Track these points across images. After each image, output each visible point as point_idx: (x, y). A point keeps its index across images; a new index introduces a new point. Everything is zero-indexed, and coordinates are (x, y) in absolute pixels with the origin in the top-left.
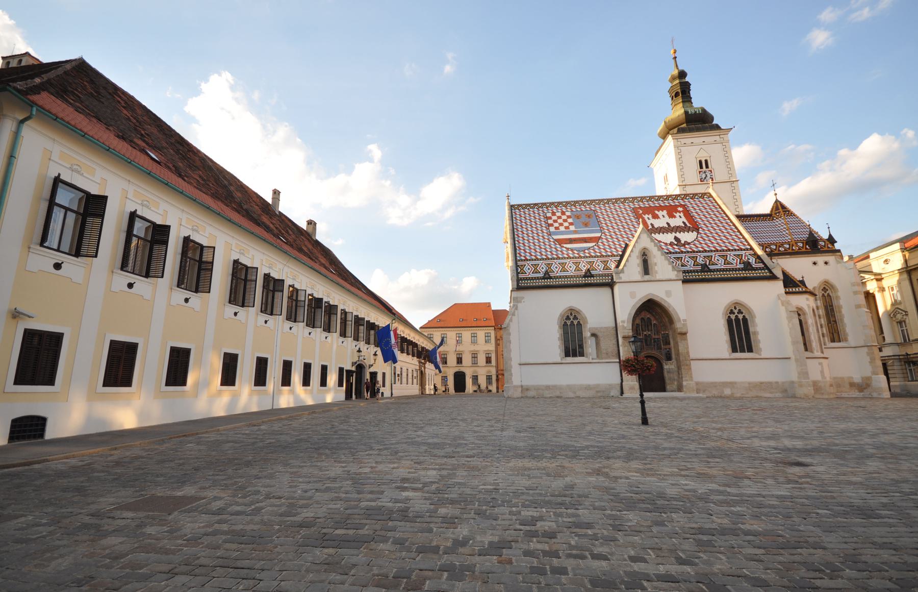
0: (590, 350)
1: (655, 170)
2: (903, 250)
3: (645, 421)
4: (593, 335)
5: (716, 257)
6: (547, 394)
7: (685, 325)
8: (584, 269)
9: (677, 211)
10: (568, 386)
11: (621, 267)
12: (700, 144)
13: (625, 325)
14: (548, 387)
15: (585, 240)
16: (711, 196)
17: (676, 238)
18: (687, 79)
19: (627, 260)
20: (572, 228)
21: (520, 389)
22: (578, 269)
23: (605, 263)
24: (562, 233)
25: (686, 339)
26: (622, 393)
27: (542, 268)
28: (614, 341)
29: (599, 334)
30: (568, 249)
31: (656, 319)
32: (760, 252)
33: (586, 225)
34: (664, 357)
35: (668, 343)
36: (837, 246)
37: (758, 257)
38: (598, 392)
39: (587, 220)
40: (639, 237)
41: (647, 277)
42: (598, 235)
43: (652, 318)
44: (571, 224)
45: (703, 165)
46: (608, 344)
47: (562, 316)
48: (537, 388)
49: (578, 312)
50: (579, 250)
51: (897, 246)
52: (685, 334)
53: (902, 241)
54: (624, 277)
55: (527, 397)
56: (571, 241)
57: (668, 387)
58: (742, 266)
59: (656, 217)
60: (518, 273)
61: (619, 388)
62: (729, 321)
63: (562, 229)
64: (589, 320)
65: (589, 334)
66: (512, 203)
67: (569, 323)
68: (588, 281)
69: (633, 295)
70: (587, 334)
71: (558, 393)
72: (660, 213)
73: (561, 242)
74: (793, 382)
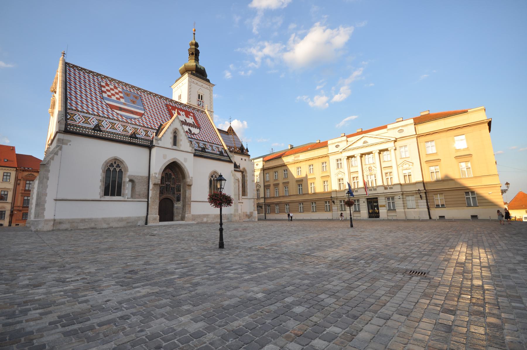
0: (127, 192)
1: (174, 90)
2: (263, 161)
3: (221, 245)
4: (131, 181)
5: (208, 146)
6: (82, 226)
7: (191, 180)
8: (130, 132)
9: (190, 115)
10: (103, 219)
11: (159, 137)
12: (199, 85)
13: (157, 176)
14: (83, 221)
16: (206, 113)
17: (189, 129)
18: (198, 49)
19: (165, 133)
20: (122, 100)
21: (52, 223)
22: (125, 130)
23: (147, 132)
24: (113, 101)
25: (190, 189)
26: (146, 223)
27: (93, 122)
28: (146, 187)
29: (136, 180)
30: (118, 114)
31: (174, 175)
32: (226, 148)
33: (134, 102)
34: (175, 199)
35: (179, 190)
36: (249, 153)
37: (225, 150)
38: (128, 223)
39: (135, 100)
40: (174, 120)
41: (175, 147)
42: (143, 112)
43: (172, 174)
44: (122, 97)
45: (200, 97)
46: (140, 188)
47: (106, 163)
48: (71, 222)
49: (122, 162)
50: (127, 118)
51: (262, 159)
52: (190, 186)
53: (263, 157)
54: (161, 143)
55: (59, 230)
56: (121, 109)
57: (175, 218)
58: (219, 153)
60: (66, 119)
61: (144, 219)
62: (211, 181)
63: (114, 98)
64: (129, 170)
65: (128, 180)
66: (67, 61)
68: (132, 140)
69: (165, 156)
70: (126, 179)
71: (93, 225)
72: (181, 113)
73: (112, 107)
74: (231, 214)
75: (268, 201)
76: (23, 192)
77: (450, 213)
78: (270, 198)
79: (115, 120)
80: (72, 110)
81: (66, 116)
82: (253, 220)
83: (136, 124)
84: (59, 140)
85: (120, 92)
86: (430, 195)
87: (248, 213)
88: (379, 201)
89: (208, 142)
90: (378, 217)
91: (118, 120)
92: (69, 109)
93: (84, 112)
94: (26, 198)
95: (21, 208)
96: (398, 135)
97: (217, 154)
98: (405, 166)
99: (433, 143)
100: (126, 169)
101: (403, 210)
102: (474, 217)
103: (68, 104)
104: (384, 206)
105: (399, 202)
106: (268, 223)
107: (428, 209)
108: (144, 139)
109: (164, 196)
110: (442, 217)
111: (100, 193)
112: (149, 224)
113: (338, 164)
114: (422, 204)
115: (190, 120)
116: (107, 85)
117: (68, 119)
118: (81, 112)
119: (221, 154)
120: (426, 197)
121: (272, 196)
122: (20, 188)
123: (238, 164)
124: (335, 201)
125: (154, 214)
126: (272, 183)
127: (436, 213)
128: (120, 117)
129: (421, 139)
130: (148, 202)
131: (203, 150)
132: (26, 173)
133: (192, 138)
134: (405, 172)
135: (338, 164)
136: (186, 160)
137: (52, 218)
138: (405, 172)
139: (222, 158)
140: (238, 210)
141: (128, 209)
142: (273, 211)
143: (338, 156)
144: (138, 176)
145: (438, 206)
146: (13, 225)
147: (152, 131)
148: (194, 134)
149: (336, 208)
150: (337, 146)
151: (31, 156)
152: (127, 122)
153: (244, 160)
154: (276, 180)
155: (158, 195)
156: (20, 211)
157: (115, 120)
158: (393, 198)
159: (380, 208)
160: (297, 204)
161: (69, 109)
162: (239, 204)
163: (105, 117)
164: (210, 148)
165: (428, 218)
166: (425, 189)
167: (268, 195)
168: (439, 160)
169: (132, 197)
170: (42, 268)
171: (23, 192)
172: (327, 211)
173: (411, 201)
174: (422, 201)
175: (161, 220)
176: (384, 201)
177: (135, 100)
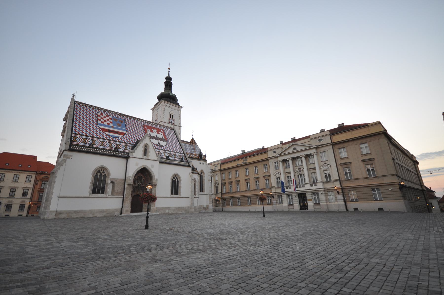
0: (108, 190)
3: (147, 227)
4: (112, 182)
6: (75, 216)
7: (157, 181)
8: (114, 147)
9: (160, 132)
14: (76, 212)
15: (117, 133)
17: (159, 143)
20: (111, 125)
22: (110, 146)
25: (156, 188)
26: (121, 214)
27: (89, 141)
28: (123, 187)
29: (115, 182)
30: (107, 135)
36: (206, 159)
38: (107, 213)
39: (120, 123)
41: (145, 157)
42: (125, 132)
43: (143, 177)
45: (172, 116)
46: (119, 188)
47: (95, 170)
48: (68, 212)
49: (106, 169)
54: (135, 155)
56: (109, 131)
59: (152, 131)
60: (71, 141)
61: (120, 211)
62: (172, 181)
63: (105, 123)
65: (109, 182)
67: (174, 180)
68: (114, 153)
71: (82, 215)
72: (154, 130)
73: (103, 130)
74: (189, 207)
75: (225, 196)
76: (39, 190)
77: (363, 206)
78: (226, 193)
79: (104, 139)
80: (76, 134)
81: (71, 139)
82: (209, 211)
83: (119, 142)
84: (64, 156)
85: (110, 119)
86: (346, 191)
87: (205, 206)
88: (307, 196)
89: (173, 152)
90: (308, 209)
91: (107, 139)
92: (74, 134)
93: (83, 135)
94: (41, 195)
95: (36, 203)
96: (319, 143)
97: (178, 161)
98: (326, 168)
99: (345, 149)
100: (109, 174)
101: (325, 204)
102: (381, 209)
103: (74, 130)
104: (311, 200)
105: (322, 197)
106: (226, 214)
107: (345, 202)
108: (123, 152)
109: (136, 193)
110: (356, 209)
111: (89, 192)
112: (123, 215)
113: (276, 166)
114: (340, 198)
115: (160, 136)
116: (102, 114)
117: (72, 141)
118: (81, 135)
119: (182, 160)
120: (343, 192)
121: (227, 192)
122: (38, 187)
123: (196, 168)
124: (275, 196)
125: (128, 207)
126: (227, 181)
127: (352, 206)
128: (108, 137)
129: (336, 146)
130: (123, 198)
131: (168, 158)
132: (42, 176)
133: (160, 149)
134: (326, 172)
135: (276, 166)
136: (153, 166)
137: (55, 210)
138: (326, 172)
139: (182, 163)
140: (193, 203)
141: (110, 203)
142: (228, 205)
143: (275, 160)
144: (117, 179)
145: (352, 201)
146: (30, 215)
147: (130, 145)
148: (162, 146)
149: (275, 202)
150: (275, 152)
151: (48, 163)
152: (113, 140)
153: (202, 163)
154: (237, 177)
155: (131, 193)
156: (36, 204)
157: (104, 139)
158: (318, 194)
159: (308, 202)
160: (370, 189)
161: (74, 134)
162: (195, 200)
163: (98, 138)
164: (174, 156)
165: (345, 210)
166: (341, 186)
167: (224, 191)
168: (350, 163)
169: (112, 194)
170: (39, 236)
171: (39, 190)
172: (269, 204)
173: (331, 196)
174: (339, 196)
175: (132, 211)
176: (311, 196)
177: (120, 123)
